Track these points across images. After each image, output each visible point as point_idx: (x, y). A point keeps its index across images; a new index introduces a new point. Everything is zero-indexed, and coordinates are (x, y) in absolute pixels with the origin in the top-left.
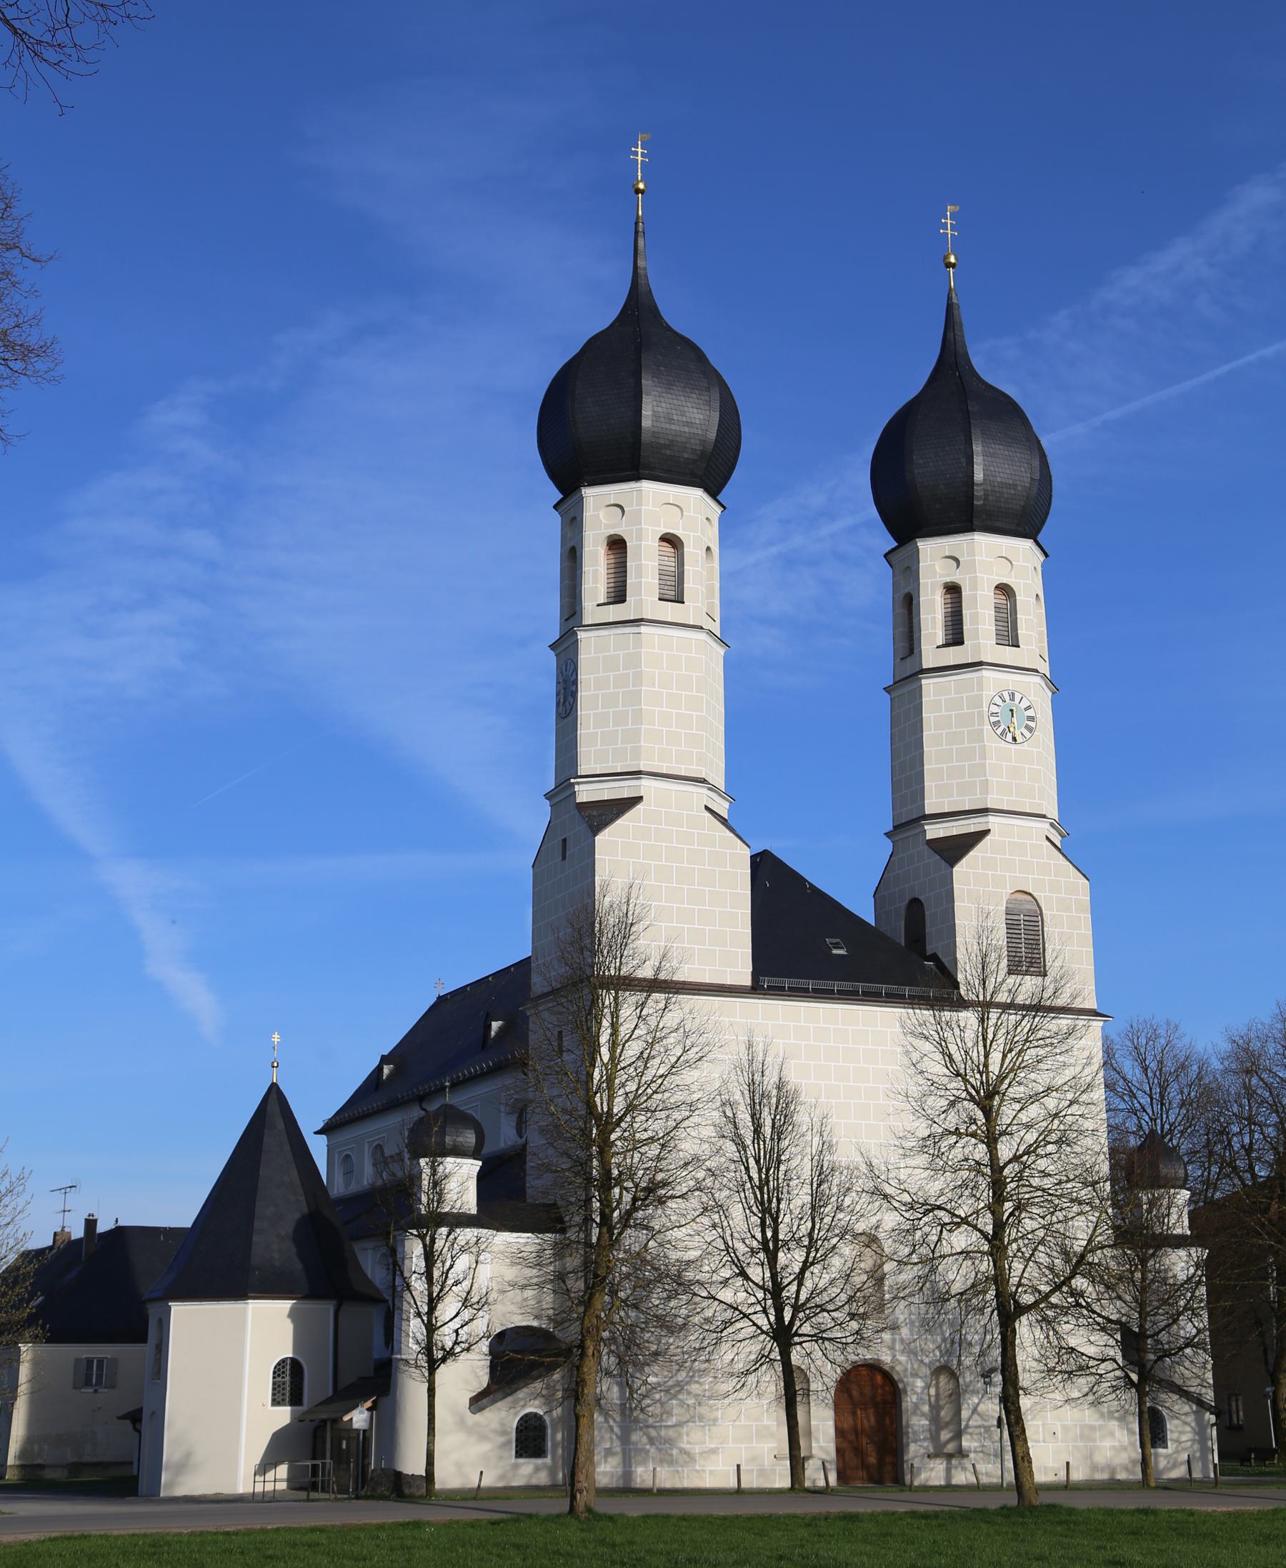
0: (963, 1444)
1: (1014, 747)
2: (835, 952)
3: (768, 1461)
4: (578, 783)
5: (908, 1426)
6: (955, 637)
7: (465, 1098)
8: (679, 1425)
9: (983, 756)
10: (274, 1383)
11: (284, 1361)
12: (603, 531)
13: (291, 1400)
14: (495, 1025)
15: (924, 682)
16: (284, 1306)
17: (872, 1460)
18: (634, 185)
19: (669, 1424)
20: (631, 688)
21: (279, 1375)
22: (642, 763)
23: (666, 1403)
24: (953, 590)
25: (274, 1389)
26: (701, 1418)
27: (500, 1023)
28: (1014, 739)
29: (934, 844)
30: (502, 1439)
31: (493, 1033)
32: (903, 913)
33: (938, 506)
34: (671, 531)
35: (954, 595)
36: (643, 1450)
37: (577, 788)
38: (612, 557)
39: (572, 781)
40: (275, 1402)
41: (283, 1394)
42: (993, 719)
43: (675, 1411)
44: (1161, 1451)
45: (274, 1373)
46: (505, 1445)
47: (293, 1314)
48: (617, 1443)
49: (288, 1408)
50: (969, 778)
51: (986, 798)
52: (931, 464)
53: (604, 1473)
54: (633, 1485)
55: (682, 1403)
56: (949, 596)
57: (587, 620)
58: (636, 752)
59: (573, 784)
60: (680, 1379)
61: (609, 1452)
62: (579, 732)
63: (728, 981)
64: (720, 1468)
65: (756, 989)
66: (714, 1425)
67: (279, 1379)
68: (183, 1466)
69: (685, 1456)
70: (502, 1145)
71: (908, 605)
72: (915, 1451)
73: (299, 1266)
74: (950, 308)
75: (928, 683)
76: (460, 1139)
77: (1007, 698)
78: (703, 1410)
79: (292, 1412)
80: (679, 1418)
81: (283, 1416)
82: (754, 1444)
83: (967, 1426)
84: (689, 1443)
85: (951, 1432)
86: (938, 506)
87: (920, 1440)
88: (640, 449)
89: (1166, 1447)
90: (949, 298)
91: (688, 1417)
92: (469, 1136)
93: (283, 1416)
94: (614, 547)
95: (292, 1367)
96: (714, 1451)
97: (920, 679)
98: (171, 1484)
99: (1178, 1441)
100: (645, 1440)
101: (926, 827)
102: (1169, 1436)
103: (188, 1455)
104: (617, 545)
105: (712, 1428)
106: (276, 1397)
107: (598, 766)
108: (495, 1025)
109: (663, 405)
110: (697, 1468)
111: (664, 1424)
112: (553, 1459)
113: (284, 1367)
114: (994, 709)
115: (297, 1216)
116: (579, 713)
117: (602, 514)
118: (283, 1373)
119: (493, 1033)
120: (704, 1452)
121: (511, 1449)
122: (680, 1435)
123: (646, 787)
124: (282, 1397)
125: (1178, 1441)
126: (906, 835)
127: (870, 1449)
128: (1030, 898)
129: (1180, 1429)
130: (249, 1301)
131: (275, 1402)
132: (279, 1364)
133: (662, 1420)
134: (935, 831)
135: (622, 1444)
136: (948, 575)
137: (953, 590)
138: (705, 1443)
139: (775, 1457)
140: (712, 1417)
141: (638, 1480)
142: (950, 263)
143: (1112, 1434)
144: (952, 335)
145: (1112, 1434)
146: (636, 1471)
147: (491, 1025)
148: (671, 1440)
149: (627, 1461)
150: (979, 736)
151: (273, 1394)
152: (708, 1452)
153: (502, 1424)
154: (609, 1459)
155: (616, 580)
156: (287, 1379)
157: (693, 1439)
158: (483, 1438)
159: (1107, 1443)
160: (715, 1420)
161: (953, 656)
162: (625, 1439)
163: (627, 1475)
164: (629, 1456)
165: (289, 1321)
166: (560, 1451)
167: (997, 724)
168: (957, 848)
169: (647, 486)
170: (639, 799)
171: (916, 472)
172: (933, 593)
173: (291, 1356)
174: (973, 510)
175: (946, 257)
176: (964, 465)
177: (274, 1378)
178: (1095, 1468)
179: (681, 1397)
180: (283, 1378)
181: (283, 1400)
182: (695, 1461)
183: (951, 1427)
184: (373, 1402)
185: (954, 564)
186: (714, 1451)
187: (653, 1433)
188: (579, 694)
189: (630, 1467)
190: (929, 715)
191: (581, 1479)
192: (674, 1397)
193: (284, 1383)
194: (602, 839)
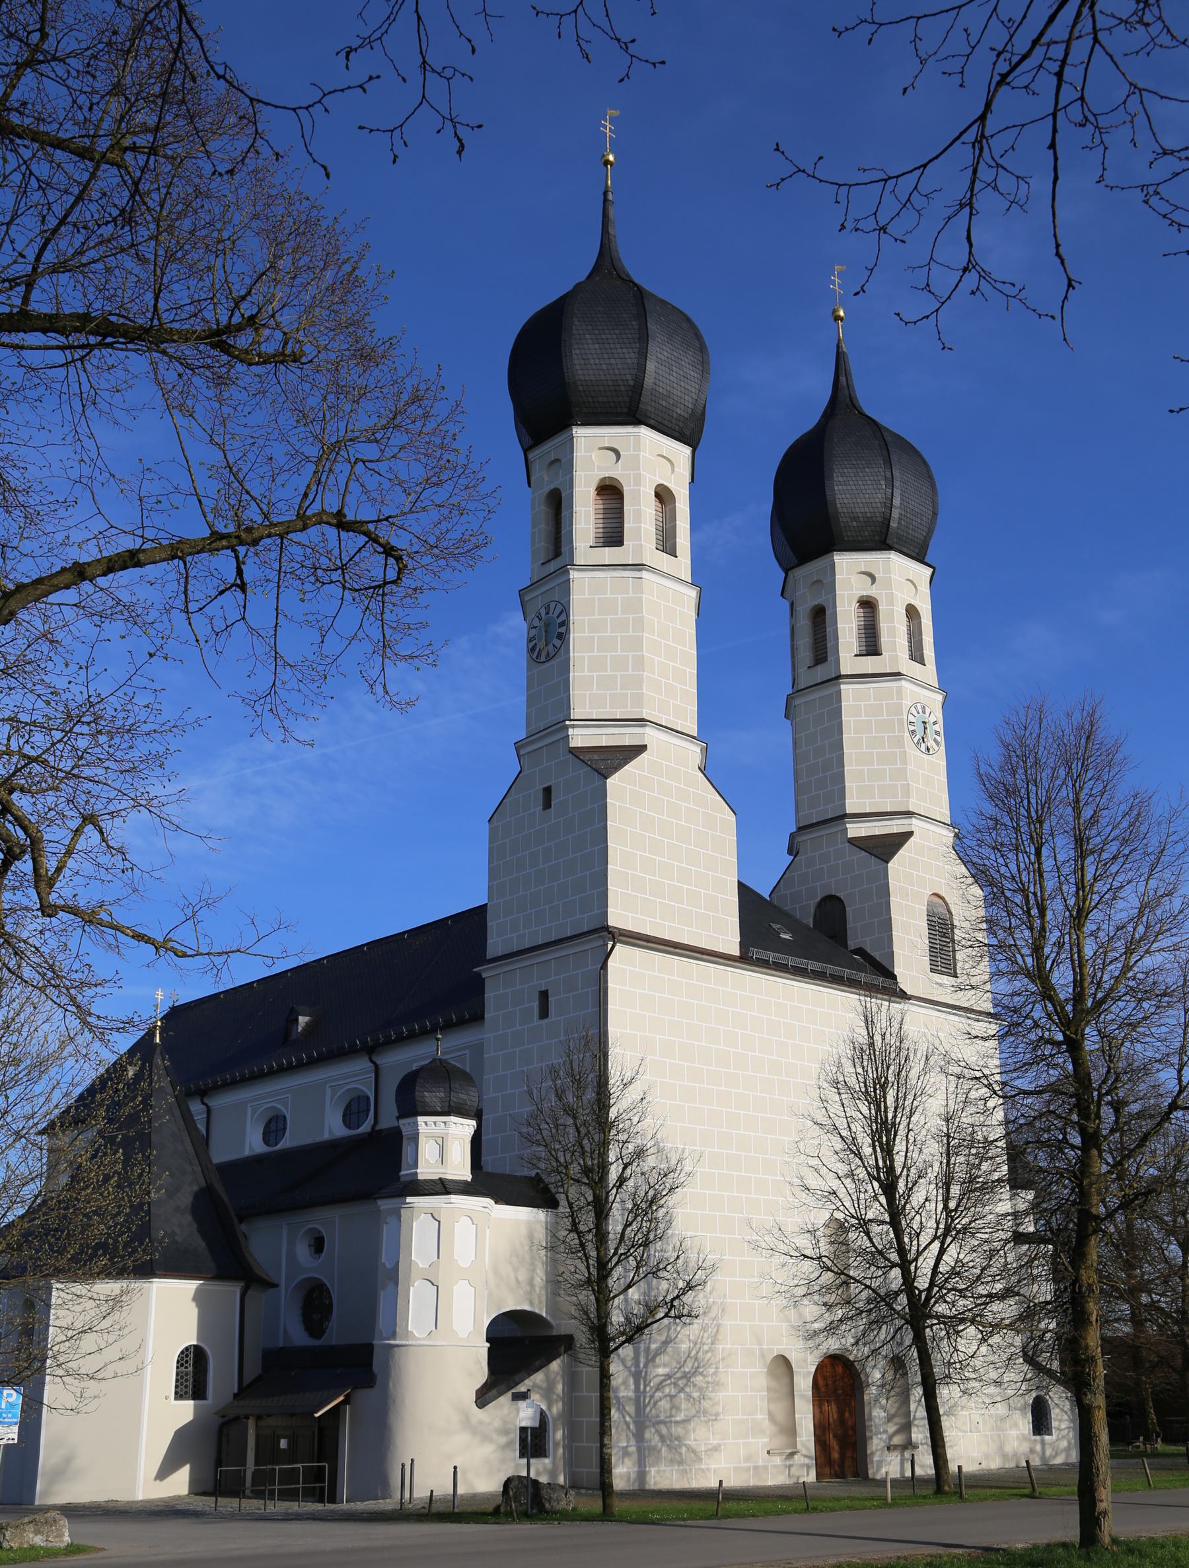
0: (913, 1435)
1: (927, 757)
2: (783, 936)
3: (762, 1459)
4: (573, 726)
5: (870, 1419)
6: (871, 646)
7: (324, 1076)
8: (686, 1421)
9: (904, 761)
10: (177, 1374)
11: (187, 1349)
12: (596, 472)
13: (194, 1393)
14: (303, 1020)
15: (843, 687)
16: (189, 1287)
17: (836, 1455)
18: (603, 156)
19: (678, 1419)
20: (631, 633)
21: (182, 1365)
22: (644, 710)
23: (675, 1396)
24: (868, 605)
25: (177, 1381)
26: (705, 1412)
27: (307, 1019)
28: (928, 749)
29: (857, 843)
30: (503, 1440)
31: (300, 1029)
32: (813, 910)
33: (854, 524)
34: (665, 484)
35: (866, 610)
36: (654, 1448)
37: (571, 731)
38: (601, 502)
39: (568, 723)
40: (179, 1396)
41: (186, 1387)
42: (912, 728)
43: (683, 1406)
44: (1047, 1437)
45: (178, 1362)
46: (509, 1445)
47: (198, 1298)
48: (633, 1442)
49: (192, 1402)
50: (890, 780)
51: (908, 802)
52: (851, 483)
53: (621, 1476)
54: (647, 1487)
55: (689, 1396)
56: (861, 610)
57: (579, 559)
58: (639, 700)
59: (567, 727)
60: (687, 1370)
61: (625, 1453)
62: (571, 674)
63: (721, 949)
64: (723, 1465)
65: (744, 959)
66: (716, 1419)
67: (183, 1369)
68: (60, 1473)
69: (692, 1455)
70: (247, 1153)
71: (821, 617)
72: (876, 1444)
73: (200, 1244)
74: (840, 357)
75: (846, 689)
76: (464, 1097)
77: (920, 711)
78: (706, 1404)
79: (196, 1407)
80: (686, 1413)
81: (186, 1410)
82: (750, 1440)
83: (915, 1418)
84: (695, 1440)
85: (896, 1424)
86: (854, 524)
87: (880, 1433)
88: (641, 394)
89: (1050, 1434)
90: (838, 347)
91: (694, 1412)
92: (473, 1094)
93: (186, 1410)
94: (602, 492)
95: (195, 1356)
96: (716, 1449)
97: (840, 684)
98: (46, 1493)
99: (1058, 1429)
100: (657, 1438)
101: (848, 826)
102: (1054, 1424)
103: (68, 1460)
104: (610, 492)
105: (714, 1423)
106: (183, 1393)
107: (594, 711)
108: (303, 1020)
109: (666, 353)
110: (703, 1467)
111: (673, 1419)
112: (554, 1463)
113: (187, 1356)
114: (911, 718)
115: (195, 1188)
116: (571, 654)
117: (595, 455)
118: (187, 1362)
119: (300, 1029)
120: (709, 1450)
121: (515, 1450)
122: (687, 1431)
123: (650, 736)
124: (183, 1393)
125: (1058, 1429)
126: (815, 835)
127: (834, 1444)
128: (941, 901)
129: (1059, 1418)
130: (155, 1280)
131: (179, 1396)
132: (182, 1352)
133: (671, 1416)
134: (855, 830)
135: (637, 1442)
136: (864, 589)
137: (868, 605)
138: (709, 1439)
139: (768, 1452)
140: (714, 1412)
141: (652, 1482)
142: (839, 316)
143: (1016, 1425)
144: (844, 379)
145: (1016, 1425)
146: (650, 1471)
147: (297, 1020)
148: (679, 1437)
149: (641, 1463)
150: (900, 742)
151: (177, 1387)
152: (711, 1450)
153: (505, 1423)
154: (626, 1460)
155: (606, 525)
156: (190, 1369)
157: (699, 1436)
158: (486, 1439)
159: (1014, 1433)
160: (717, 1414)
161: (870, 664)
162: (639, 1437)
163: (642, 1475)
164: (644, 1455)
165: (194, 1304)
166: (561, 1451)
167: (913, 732)
168: (887, 847)
169: (644, 431)
170: (642, 748)
171: (836, 488)
172: (850, 604)
173: (195, 1343)
174: (888, 530)
175: (835, 311)
176: (884, 487)
177: (177, 1367)
178: (1005, 1456)
179: (687, 1390)
180: (186, 1368)
181: (186, 1393)
182: (701, 1460)
183: (896, 1420)
184: (346, 1396)
185: (869, 580)
186: (716, 1449)
187: (664, 1430)
188: (571, 635)
189: (645, 1467)
190: (848, 719)
191: (1104, 1497)
192: (682, 1390)
193: (187, 1374)
194: (613, 782)
